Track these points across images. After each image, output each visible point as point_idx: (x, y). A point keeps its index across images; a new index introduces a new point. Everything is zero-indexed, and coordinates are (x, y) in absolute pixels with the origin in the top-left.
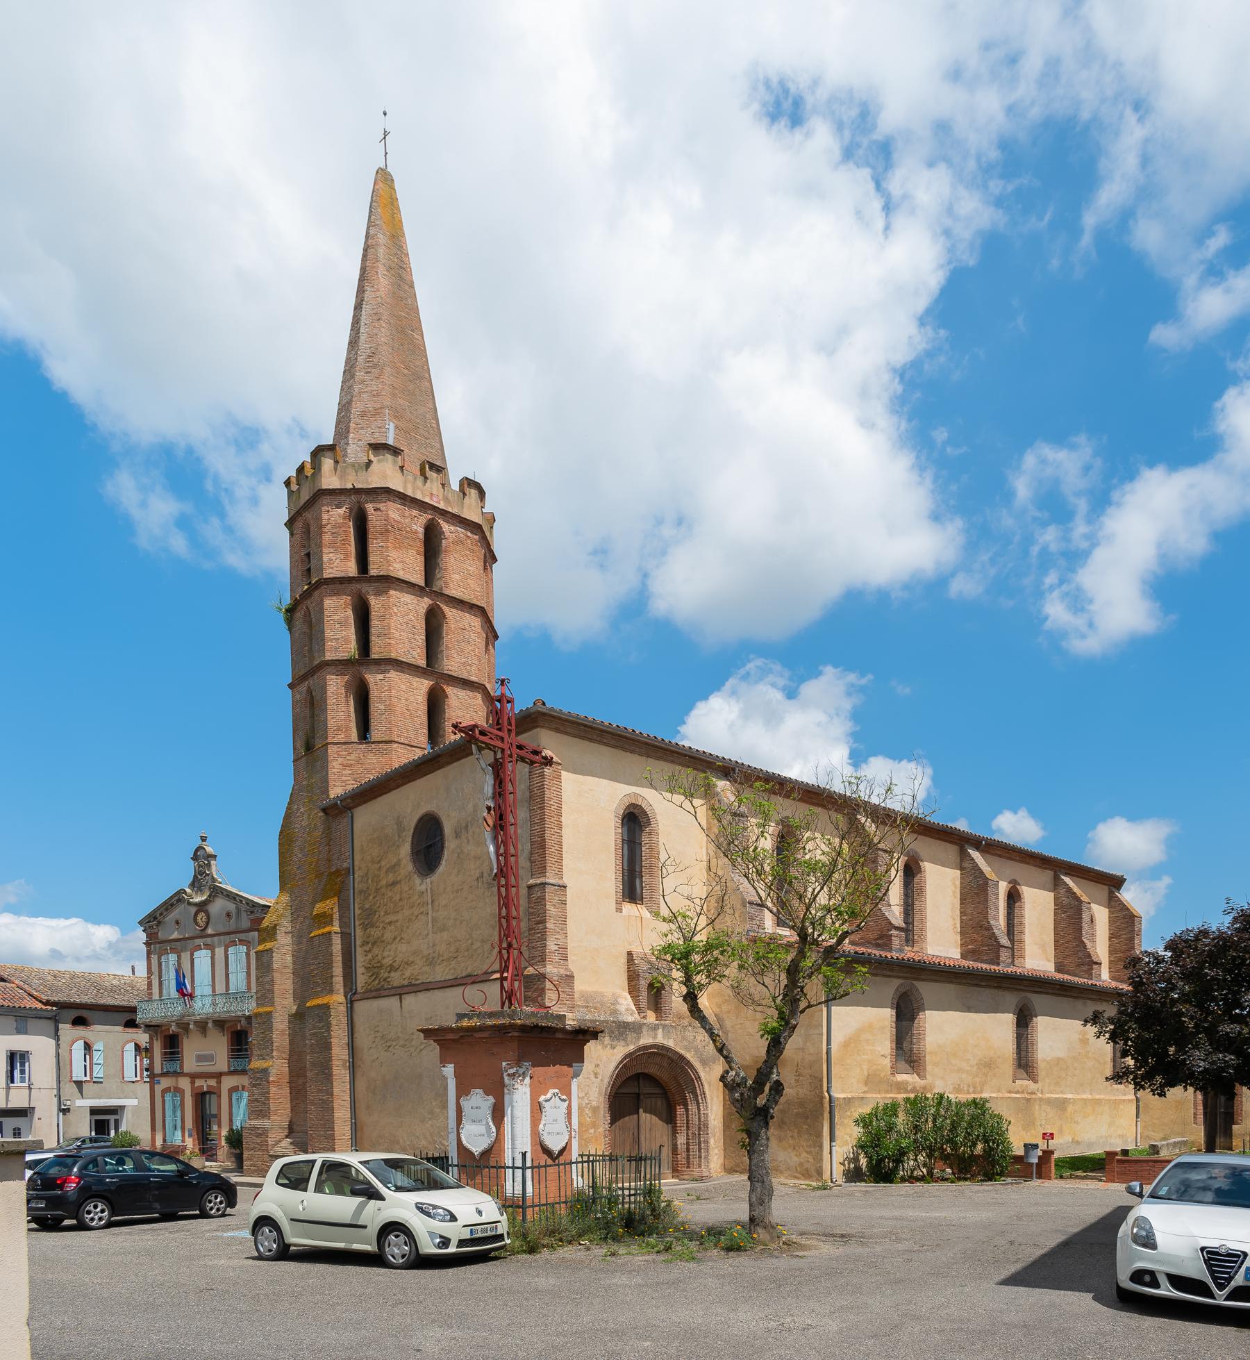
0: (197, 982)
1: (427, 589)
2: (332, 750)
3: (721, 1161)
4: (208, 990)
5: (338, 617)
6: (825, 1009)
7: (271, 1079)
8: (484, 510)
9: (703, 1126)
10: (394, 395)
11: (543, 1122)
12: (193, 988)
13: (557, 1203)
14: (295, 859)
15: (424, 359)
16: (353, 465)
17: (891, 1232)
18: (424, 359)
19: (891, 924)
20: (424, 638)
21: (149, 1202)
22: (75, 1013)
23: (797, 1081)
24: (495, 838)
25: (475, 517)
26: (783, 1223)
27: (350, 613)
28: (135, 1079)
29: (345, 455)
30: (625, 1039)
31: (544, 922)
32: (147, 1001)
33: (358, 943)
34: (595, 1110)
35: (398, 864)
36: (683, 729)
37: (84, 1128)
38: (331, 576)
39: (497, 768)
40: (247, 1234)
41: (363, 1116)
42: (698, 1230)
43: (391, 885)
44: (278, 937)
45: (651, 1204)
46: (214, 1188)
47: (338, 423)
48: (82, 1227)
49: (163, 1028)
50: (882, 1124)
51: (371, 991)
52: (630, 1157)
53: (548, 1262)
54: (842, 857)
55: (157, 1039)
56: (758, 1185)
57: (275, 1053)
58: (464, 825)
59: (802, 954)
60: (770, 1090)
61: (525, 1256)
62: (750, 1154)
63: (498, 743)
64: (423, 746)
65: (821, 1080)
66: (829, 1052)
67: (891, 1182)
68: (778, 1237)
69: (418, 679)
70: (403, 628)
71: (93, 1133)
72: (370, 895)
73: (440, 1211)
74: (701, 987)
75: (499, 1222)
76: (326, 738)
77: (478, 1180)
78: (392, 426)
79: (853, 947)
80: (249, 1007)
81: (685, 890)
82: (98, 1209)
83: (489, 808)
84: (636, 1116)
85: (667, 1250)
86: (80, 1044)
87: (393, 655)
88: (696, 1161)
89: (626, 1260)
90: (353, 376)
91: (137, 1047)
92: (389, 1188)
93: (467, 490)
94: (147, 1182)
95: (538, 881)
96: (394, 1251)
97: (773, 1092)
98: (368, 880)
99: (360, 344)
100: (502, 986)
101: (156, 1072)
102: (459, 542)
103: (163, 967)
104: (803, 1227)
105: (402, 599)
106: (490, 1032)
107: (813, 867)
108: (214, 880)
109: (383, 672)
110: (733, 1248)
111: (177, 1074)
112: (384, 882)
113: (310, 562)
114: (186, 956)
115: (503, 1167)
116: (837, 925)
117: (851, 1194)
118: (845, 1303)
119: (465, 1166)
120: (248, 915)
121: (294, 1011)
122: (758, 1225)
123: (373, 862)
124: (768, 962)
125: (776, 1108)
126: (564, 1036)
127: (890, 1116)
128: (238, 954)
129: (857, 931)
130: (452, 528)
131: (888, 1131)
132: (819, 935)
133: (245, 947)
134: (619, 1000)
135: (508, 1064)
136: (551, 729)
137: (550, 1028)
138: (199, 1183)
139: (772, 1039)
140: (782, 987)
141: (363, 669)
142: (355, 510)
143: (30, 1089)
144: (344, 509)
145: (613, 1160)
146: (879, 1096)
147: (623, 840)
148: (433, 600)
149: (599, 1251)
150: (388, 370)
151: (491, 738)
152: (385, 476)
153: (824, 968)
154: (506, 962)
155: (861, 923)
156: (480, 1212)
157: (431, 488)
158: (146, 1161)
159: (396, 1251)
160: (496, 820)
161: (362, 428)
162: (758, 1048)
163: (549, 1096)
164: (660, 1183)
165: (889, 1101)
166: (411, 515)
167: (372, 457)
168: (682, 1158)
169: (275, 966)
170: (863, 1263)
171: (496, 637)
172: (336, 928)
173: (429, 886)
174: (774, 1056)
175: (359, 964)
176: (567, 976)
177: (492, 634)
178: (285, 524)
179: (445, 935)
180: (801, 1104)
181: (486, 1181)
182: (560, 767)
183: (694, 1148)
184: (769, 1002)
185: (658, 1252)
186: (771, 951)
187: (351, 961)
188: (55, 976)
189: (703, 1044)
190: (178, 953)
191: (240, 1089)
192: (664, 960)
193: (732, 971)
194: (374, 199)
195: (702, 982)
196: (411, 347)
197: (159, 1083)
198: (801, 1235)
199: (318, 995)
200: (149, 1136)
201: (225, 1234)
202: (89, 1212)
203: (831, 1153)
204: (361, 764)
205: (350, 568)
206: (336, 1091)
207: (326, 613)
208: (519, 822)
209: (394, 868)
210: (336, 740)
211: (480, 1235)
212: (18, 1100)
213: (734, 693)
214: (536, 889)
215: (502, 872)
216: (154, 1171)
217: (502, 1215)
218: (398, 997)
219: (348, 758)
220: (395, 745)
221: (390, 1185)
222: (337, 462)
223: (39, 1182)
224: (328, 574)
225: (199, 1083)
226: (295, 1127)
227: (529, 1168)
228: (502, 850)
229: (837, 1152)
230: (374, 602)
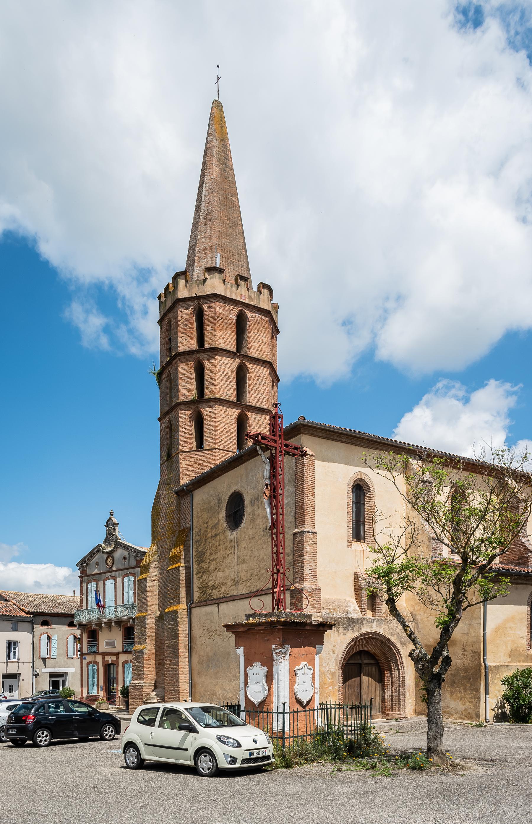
0: (107, 599)
1: (238, 354)
2: (182, 456)
3: (413, 707)
4: (113, 604)
5: (186, 375)
6: (482, 607)
7: (145, 656)
8: (272, 302)
9: (401, 685)
10: (221, 237)
11: (297, 683)
12: (104, 602)
13: (304, 736)
14: (160, 523)
15: (238, 213)
16: (196, 282)
17: (525, 759)
18: (238, 213)
19: (527, 549)
20: (235, 384)
21: (72, 730)
22: (42, 619)
23: (463, 655)
24: (270, 504)
25: (266, 306)
26: (451, 751)
27: (193, 372)
28: (73, 656)
29: (192, 277)
30: (353, 629)
31: (302, 555)
32: (80, 611)
33: (195, 572)
34: (333, 674)
35: (218, 523)
36: (396, 431)
37: (45, 685)
38: (183, 350)
39: (272, 460)
40: (120, 751)
41: (196, 678)
42: (395, 754)
43: (214, 536)
44: (150, 570)
45: (365, 736)
46: (108, 722)
47: (189, 257)
48: (35, 745)
49: (88, 626)
50: (521, 683)
51: (201, 602)
52: (352, 705)
53: (297, 774)
54: (491, 505)
55: (85, 633)
56: (434, 726)
57: (147, 641)
58: (256, 497)
59: (464, 570)
60: (442, 662)
61: (284, 770)
62: (428, 704)
63: (273, 444)
64: (234, 451)
65: (479, 654)
66: (484, 636)
67: (527, 722)
68: (447, 761)
69: (231, 409)
70: (223, 379)
71: (51, 688)
72: (201, 543)
73: (231, 741)
74: (398, 594)
75: (267, 748)
76: (179, 449)
77: (256, 720)
78: (219, 256)
79: (502, 566)
80: (134, 613)
81: (388, 532)
82: (44, 735)
83: (267, 485)
84: (359, 678)
85: (373, 768)
86: (45, 636)
87: (217, 396)
88: (397, 707)
89: (346, 774)
90: (197, 228)
91: (75, 637)
92: (201, 726)
93: (262, 290)
94: (71, 719)
95: (300, 530)
96: (203, 765)
97: (444, 664)
98: (201, 534)
99: (202, 208)
100: (273, 597)
101: (84, 652)
102: (257, 323)
103: (89, 590)
104: (464, 754)
106: (265, 626)
107: (472, 512)
108: (117, 538)
109: (212, 406)
110: (416, 768)
111: (95, 653)
112: (210, 535)
113: (171, 344)
114: (101, 583)
115: (271, 712)
116: (489, 551)
117: (499, 731)
118: (489, 810)
119: (248, 711)
120: (135, 558)
121: (158, 615)
122: (433, 752)
123: (204, 523)
124: (442, 577)
125: (446, 675)
126: (311, 628)
127: (526, 678)
128: (129, 581)
129: (502, 554)
130: (253, 315)
131: (525, 688)
132: (477, 558)
133: (133, 577)
134: (349, 604)
135: (276, 647)
137: (302, 623)
138: (100, 719)
139: (444, 628)
140: (451, 594)
141: (200, 406)
142: (197, 309)
143: (18, 663)
145: (341, 708)
146: (518, 664)
147: (353, 502)
148: (241, 360)
149: (330, 767)
150: (217, 222)
151: (269, 441)
152: (214, 287)
153: (479, 579)
154: (276, 582)
155: (505, 549)
156: (255, 742)
157: (241, 291)
158: (71, 706)
159: (205, 765)
160: (271, 492)
161: (202, 259)
162: (436, 633)
163: (301, 666)
164: (371, 721)
165: (526, 668)
166: (229, 309)
167: (207, 276)
168: (388, 705)
169: (148, 588)
170: (504, 781)
171: (278, 380)
172: (183, 564)
173: (236, 536)
174: (445, 639)
175: (195, 586)
176: (316, 589)
177: (275, 379)
178: (158, 322)
179: (244, 566)
180: (466, 670)
181: (261, 721)
182: (314, 458)
183: (396, 699)
184: (442, 603)
185: (367, 769)
186: (444, 569)
187: (191, 584)
188: (33, 597)
190: (97, 582)
191: (129, 662)
192: (374, 577)
193: (418, 584)
194: (211, 119)
195: (398, 591)
197: (85, 659)
198: (463, 759)
199: (171, 605)
200: (80, 690)
201: (112, 751)
202: (39, 737)
203: (485, 703)
205: (194, 345)
206: (181, 663)
207: (180, 373)
208: (286, 493)
209: (215, 526)
210: (184, 450)
211: (255, 756)
212: (12, 669)
213: (427, 404)
214: (298, 535)
215: (275, 525)
216: (75, 712)
217: (269, 743)
218: (216, 605)
219: (191, 460)
220: (218, 451)
221: (202, 724)
222: (187, 281)
223: (13, 718)
225: (107, 658)
226: (158, 685)
227: (287, 713)
228: (274, 511)
229: (489, 702)
230: (207, 364)
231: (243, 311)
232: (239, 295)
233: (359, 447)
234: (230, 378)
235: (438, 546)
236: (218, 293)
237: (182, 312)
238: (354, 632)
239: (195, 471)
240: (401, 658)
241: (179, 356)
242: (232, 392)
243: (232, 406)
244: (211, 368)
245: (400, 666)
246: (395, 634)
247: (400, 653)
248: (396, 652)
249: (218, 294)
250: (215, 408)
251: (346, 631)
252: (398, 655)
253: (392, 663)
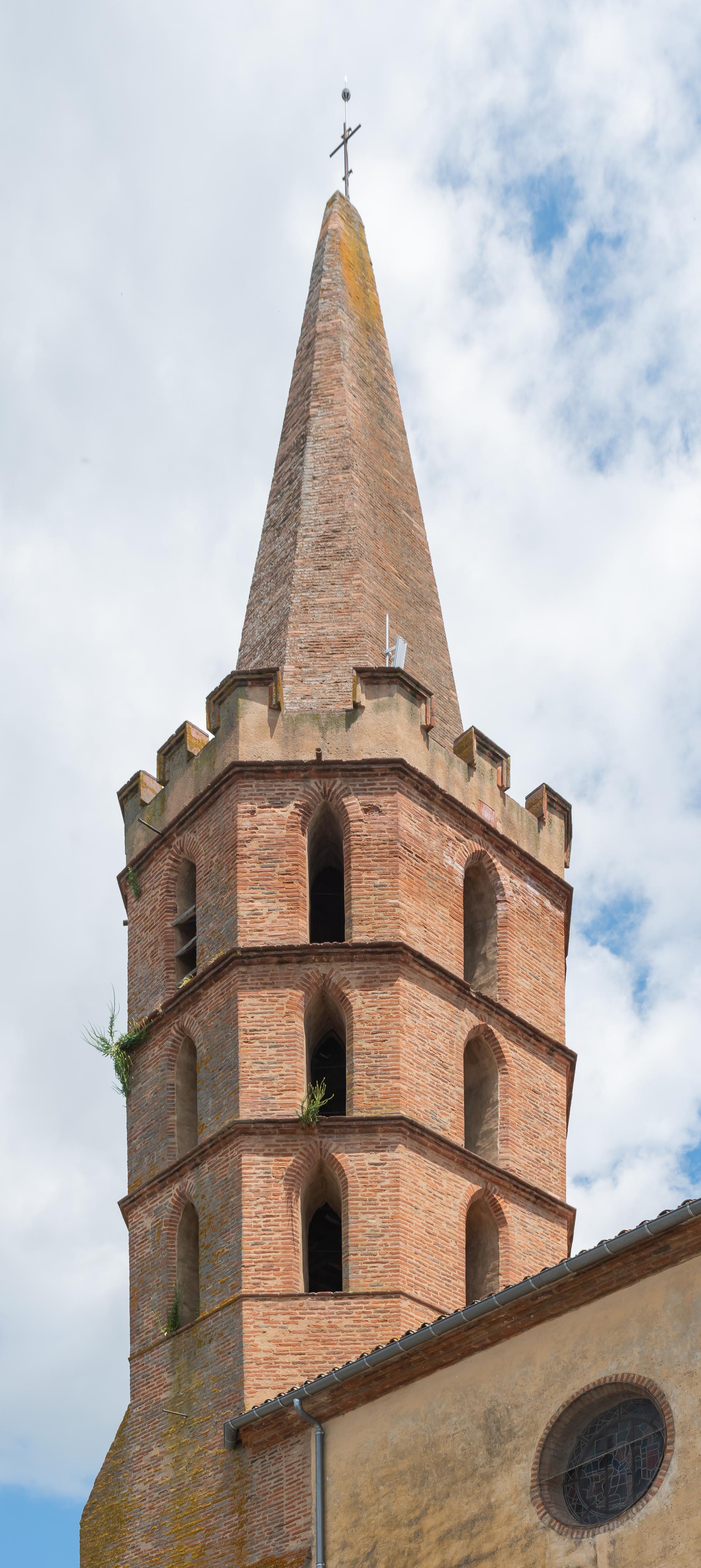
2: (250, 1311)
5: (273, 1034)
27: (300, 1025)
35: (488, 1514)
69: (450, 1174)
70: (423, 1062)
99: (303, 515)
102: (528, 914)
105: (422, 1003)
130: (518, 882)
141: (332, 1144)
142: (316, 813)
144: (291, 807)
148: (481, 1018)
150: (367, 567)
157: (481, 790)
161: (313, 674)
167: (362, 698)
196: (407, 540)
204: (324, 1342)
207: (243, 1024)
210: (262, 1290)
219: (291, 1327)
220: (405, 1303)
222: (276, 708)
224: (248, 939)
231: (484, 861)
234: (446, 1068)
237: (253, 812)
239: (309, 1367)
241: (243, 964)
242: (452, 1116)
243: (452, 1163)
244: (378, 1019)
250: (397, 1156)
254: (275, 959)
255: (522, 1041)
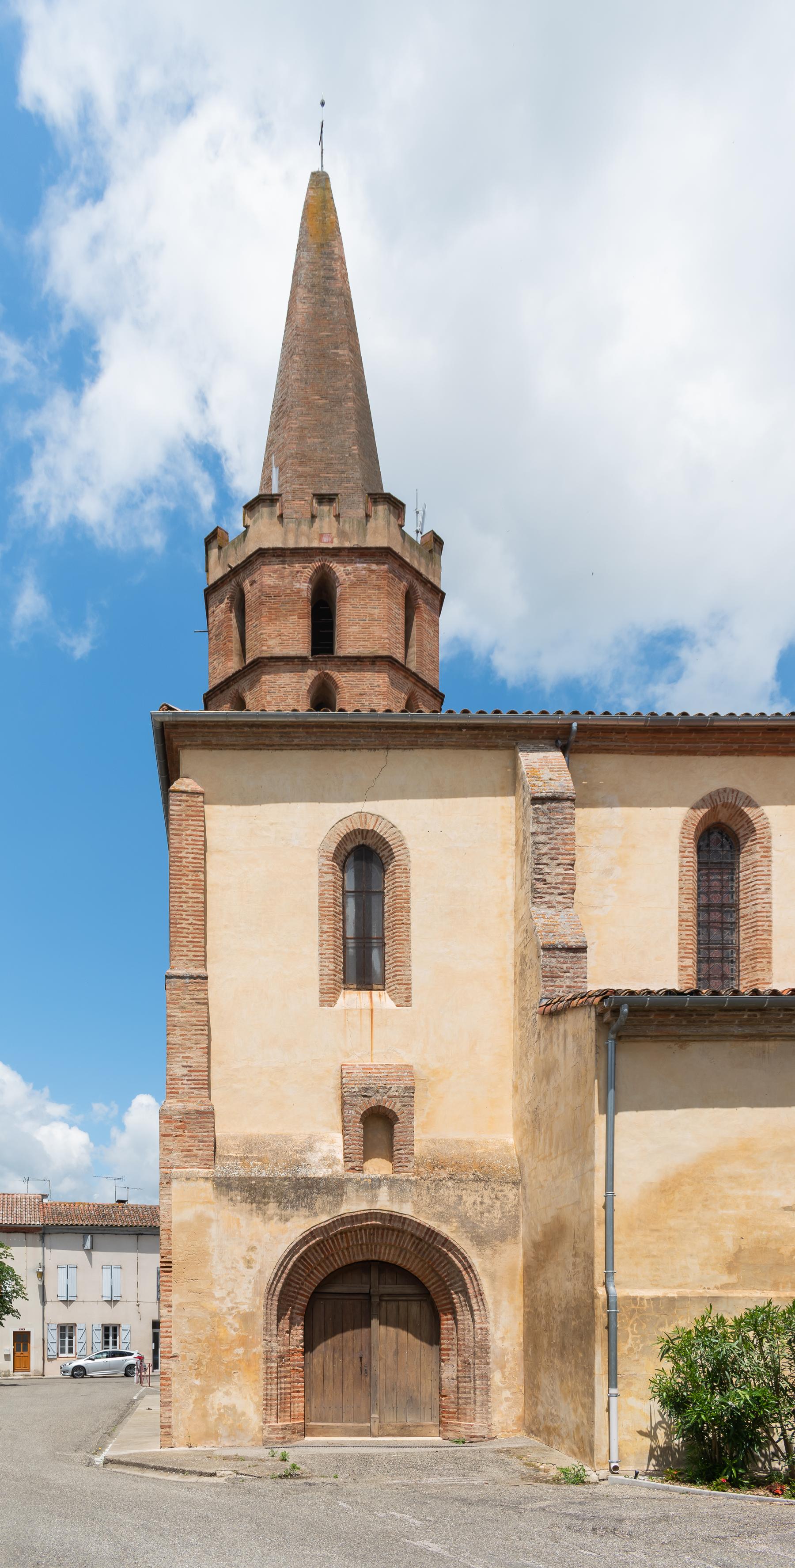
3: (519, 1411)
9: (483, 1349)
66: (609, 1206)
84: (365, 1331)
102: (360, 582)
105: (278, 682)
130: (349, 568)
136: (197, 747)
157: (321, 527)
166: (292, 572)
167: (249, 522)
176: (199, 1112)
189: (479, 1208)
231: (325, 569)
232: (316, 536)
233: (357, 752)
235: (565, 966)
236: (266, 545)
238: (316, 1215)
240: (476, 1280)
245: (473, 1301)
246: (455, 1216)
247: (470, 1267)
248: (459, 1265)
249: (265, 549)
251: (289, 1212)
252: (468, 1273)
253: (456, 1293)
254: (219, 692)
255: (351, 667)
